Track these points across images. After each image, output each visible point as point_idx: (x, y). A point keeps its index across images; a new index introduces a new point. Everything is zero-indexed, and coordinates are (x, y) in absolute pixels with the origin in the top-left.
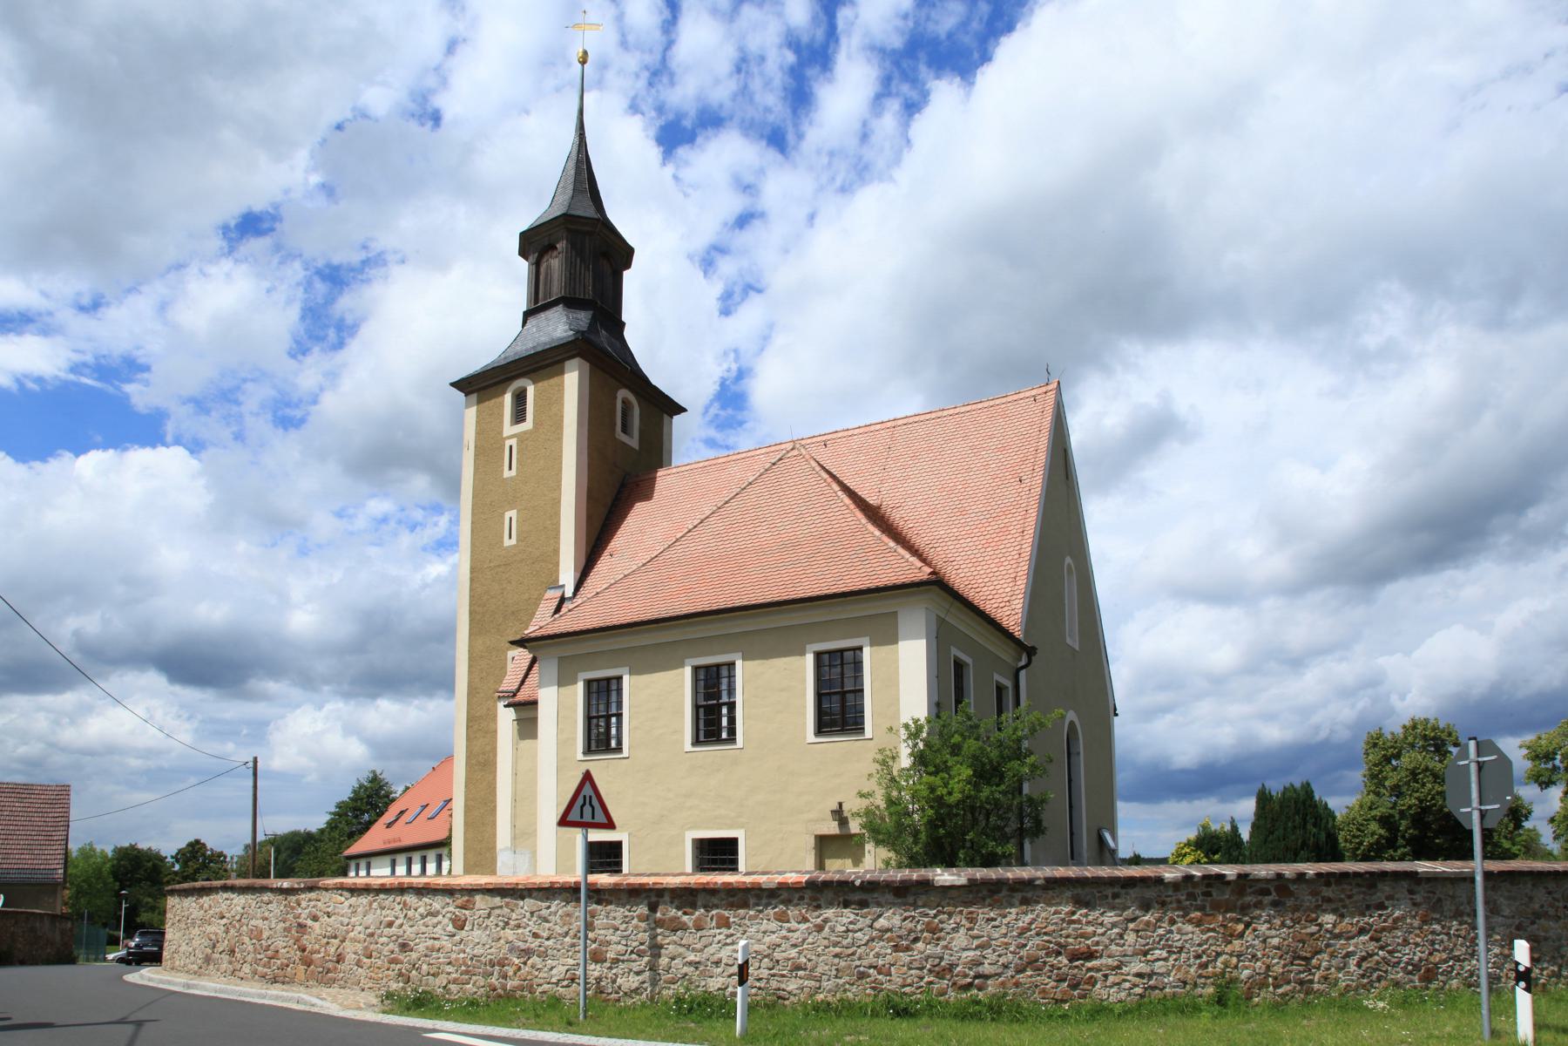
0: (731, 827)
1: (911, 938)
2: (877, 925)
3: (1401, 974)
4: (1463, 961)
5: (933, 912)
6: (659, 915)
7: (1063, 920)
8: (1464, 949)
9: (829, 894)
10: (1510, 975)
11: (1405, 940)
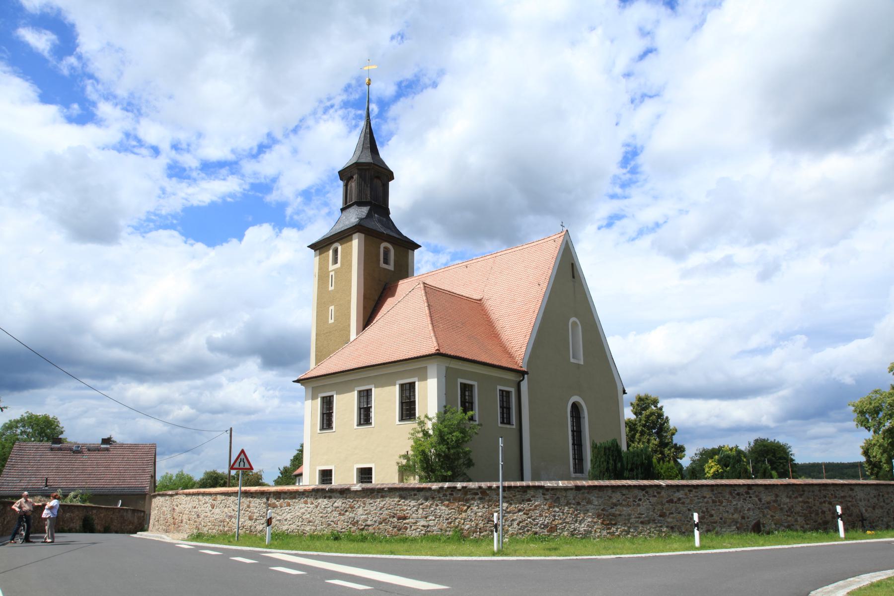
0: (369, 462)
1: (345, 510)
2: (334, 505)
3: (119, 506)
4: (571, 524)
5: (352, 501)
6: (269, 502)
7: (396, 504)
8: (571, 519)
9: (320, 494)
10: (597, 530)
11: (540, 515)
